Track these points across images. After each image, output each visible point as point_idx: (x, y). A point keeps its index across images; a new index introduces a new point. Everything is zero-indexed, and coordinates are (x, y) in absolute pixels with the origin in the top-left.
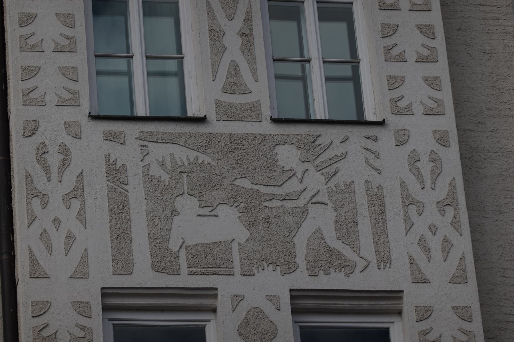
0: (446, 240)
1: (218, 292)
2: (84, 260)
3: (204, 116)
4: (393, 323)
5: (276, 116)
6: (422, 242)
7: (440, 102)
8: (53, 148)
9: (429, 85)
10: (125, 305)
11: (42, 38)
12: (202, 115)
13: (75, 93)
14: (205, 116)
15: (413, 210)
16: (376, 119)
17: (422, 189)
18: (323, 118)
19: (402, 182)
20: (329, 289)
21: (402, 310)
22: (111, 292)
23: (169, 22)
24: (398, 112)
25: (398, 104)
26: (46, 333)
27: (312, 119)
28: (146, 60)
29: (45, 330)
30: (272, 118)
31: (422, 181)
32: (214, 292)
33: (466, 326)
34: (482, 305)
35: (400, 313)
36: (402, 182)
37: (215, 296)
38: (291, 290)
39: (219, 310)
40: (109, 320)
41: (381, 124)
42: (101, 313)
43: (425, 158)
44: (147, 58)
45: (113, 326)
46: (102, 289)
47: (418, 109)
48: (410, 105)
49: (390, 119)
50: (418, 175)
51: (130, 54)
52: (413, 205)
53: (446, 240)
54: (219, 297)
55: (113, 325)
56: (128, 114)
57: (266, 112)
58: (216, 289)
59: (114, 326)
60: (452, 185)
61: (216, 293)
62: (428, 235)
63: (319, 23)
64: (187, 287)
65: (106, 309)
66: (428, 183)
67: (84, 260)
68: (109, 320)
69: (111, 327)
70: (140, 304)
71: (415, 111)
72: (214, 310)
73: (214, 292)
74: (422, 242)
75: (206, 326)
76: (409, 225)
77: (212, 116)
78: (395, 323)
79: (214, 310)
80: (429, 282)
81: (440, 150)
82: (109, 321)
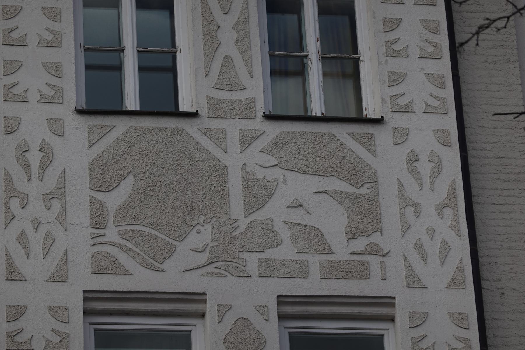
0: (445, 243)
1: (206, 297)
2: (65, 262)
3: (380, 117)
4: (195, 326)
5: (267, 113)
6: (419, 246)
8: (35, 146)
10: (187, 311)
12: (194, 110)
15: (410, 211)
16: (192, 111)
18: (134, 109)
19: (7, 174)
20: (360, 296)
23: (295, 17)
26: (424, 345)
28: (84, 51)
29: (19, 335)
32: (392, 301)
33: (463, 333)
36: (7, 174)
37: (393, 305)
38: (84, 292)
40: (90, 324)
41: (378, 121)
42: (277, 320)
43: (35, 146)
44: (86, 50)
45: (95, 331)
46: (278, 297)
51: (303, 52)
52: (448, 208)
53: (445, 243)
56: (302, 113)
57: (260, 108)
59: (290, 333)
61: (205, 298)
62: (425, 239)
63: (136, 10)
64: (189, 292)
65: (87, 313)
67: (65, 262)
68: (90, 324)
69: (93, 332)
70: (111, 308)
71: (415, 109)
72: (392, 319)
73: (392, 301)
74: (419, 246)
76: (406, 228)
77: (204, 112)
80: (24, 279)
82: (90, 325)
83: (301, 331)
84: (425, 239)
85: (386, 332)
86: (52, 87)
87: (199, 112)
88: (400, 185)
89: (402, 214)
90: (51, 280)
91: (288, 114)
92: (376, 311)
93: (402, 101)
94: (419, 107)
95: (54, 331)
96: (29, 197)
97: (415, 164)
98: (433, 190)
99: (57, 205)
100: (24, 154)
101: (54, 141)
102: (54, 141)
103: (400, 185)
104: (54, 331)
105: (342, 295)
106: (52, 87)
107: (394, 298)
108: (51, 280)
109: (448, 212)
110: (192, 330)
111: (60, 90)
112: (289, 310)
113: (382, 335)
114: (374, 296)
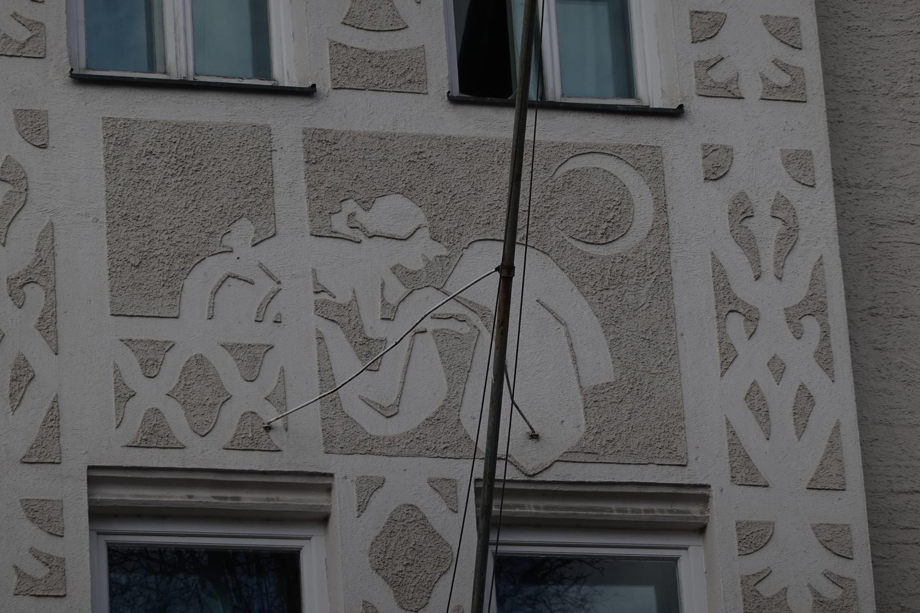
2: (53, 419)
4: (686, 549)
7: (796, 74)
9: (775, 34)
11: (186, 445)
12: (308, 84)
13: (36, 27)
15: (736, 324)
24: (711, 91)
25: (761, 588)
32: (705, 492)
34: (862, 421)
35: (701, 530)
37: (328, 489)
39: (334, 521)
41: (676, 113)
43: (763, 208)
45: (113, 565)
47: (752, 88)
48: (736, 79)
50: (748, 244)
54: (335, 491)
62: (766, 381)
67: (53, 419)
75: (301, 549)
76: (728, 356)
77: (325, 85)
78: (690, 549)
79: (323, 520)
82: (99, 536)
84: (766, 381)
85: (683, 551)
86: (784, 68)
87: (318, 87)
89: (722, 328)
94: (752, 88)
95: (827, 575)
99: (35, 295)
100: (745, 223)
104: (827, 575)
106: (784, 68)
107: (332, 475)
109: (811, 326)
110: (304, 548)
112: (112, 495)
113: (675, 560)
114: (277, 471)
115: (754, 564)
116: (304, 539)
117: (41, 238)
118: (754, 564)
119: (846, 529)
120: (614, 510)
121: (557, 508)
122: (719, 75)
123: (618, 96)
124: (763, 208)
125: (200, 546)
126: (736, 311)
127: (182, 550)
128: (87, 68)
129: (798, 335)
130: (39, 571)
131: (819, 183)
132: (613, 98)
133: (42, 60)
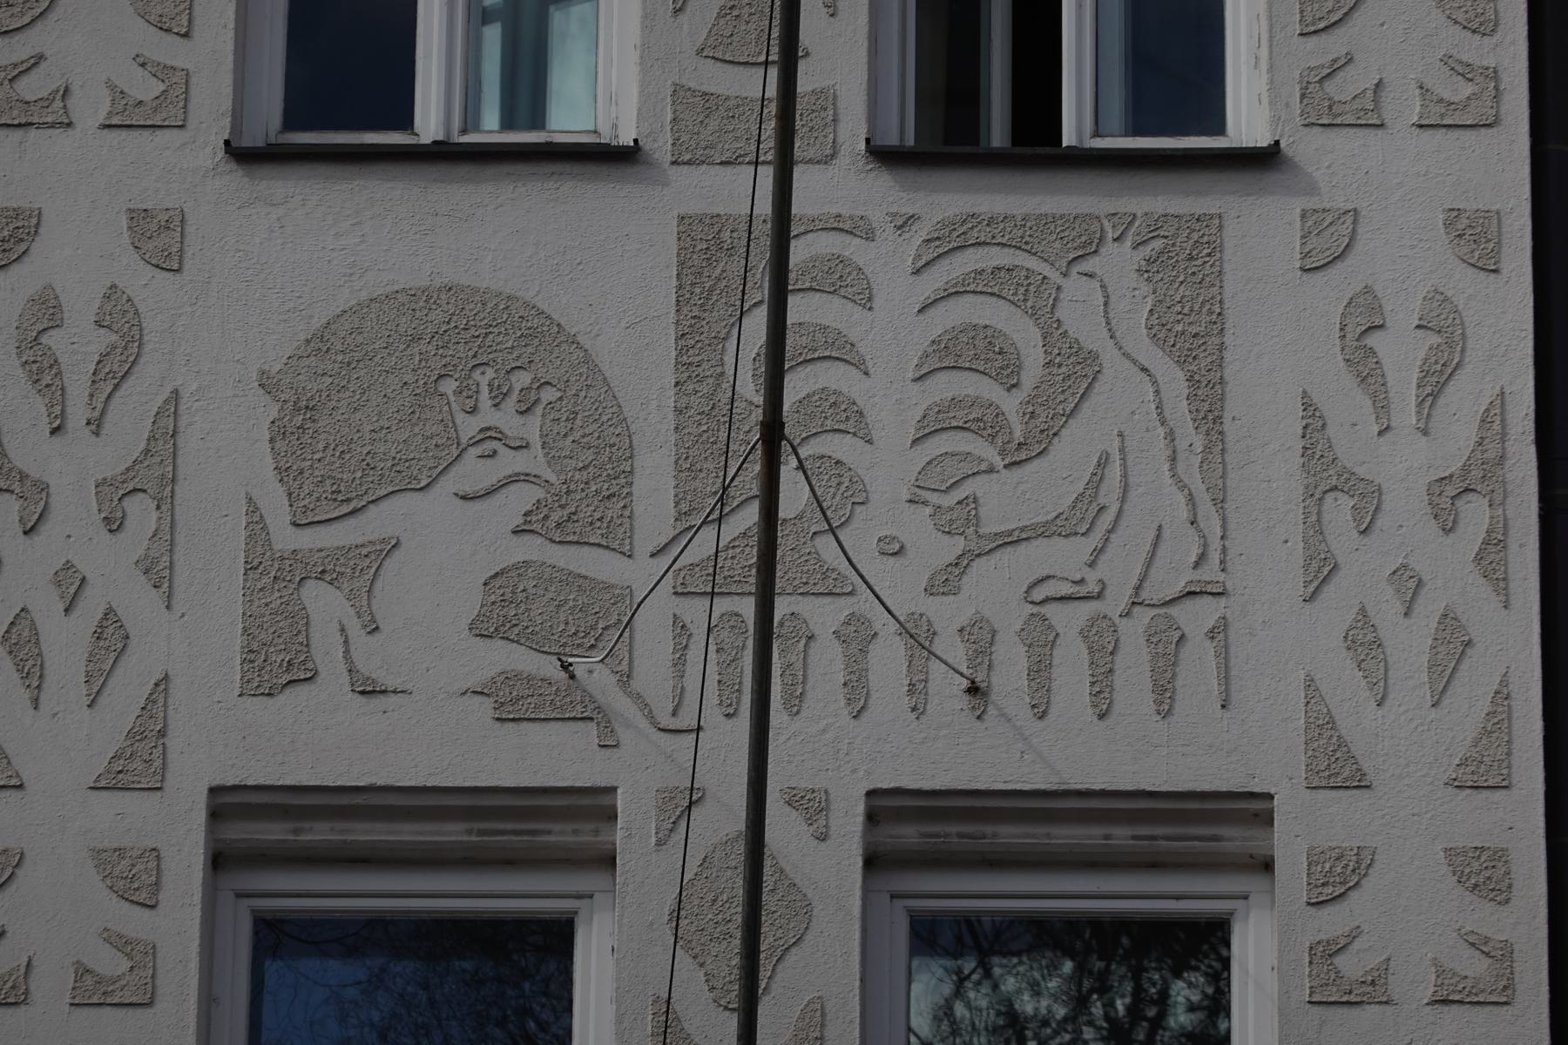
4: (1246, 898)
14: (1277, 143)
15: (1339, 510)
17: (54, 431)
21: (1272, 859)
22: (1262, 807)
27: (993, 148)
30: (872, 143)
31: (1382, 407)
32: (604, 800)
35: (607, 861)
37: (1266, 819)
40: (240, 895)
43: (81, 306)
46: (214, 791)
49: (1303, 147)
55: (908, 911)
58: (1270, 797)
60: (1493, 417)
62: (1387, 612)
66: (78, 413)
68: (240, 895)
77: (660, 148)
78: (596, 896)
81: (1464, 284)
83: (1219, 907)
88: (1313, 419)
90: (112, 783)
91: (886, 144)
92: (1019, 837)
93: (1346, 87)
96: (1423, 592)
97: (1373, 340)
98: (1425, 432)
101: (145, 285)
102: (145, 285)
103: (1313, 419)
105: (578, 784)
108: (112, 783)
111: (177, 84)
112: (239, 832)
115: (1332, 922)
116: (579, 897)
117: (1485, 421)
118: (1332, 922)
119: (1499, 856)
120: (1010, 835)
121: (515, 833)
122: (1346, 87)
123: (1137, 130)
124: (1402, 312)
125: (944, 912)
126: (1472, 490)
127: (973, 918)
128: (464, 131)
129: (114, 525)
130: (111, 963)
131: (1506, 267)
132: (1126, 135)
133: (1490, 131)
